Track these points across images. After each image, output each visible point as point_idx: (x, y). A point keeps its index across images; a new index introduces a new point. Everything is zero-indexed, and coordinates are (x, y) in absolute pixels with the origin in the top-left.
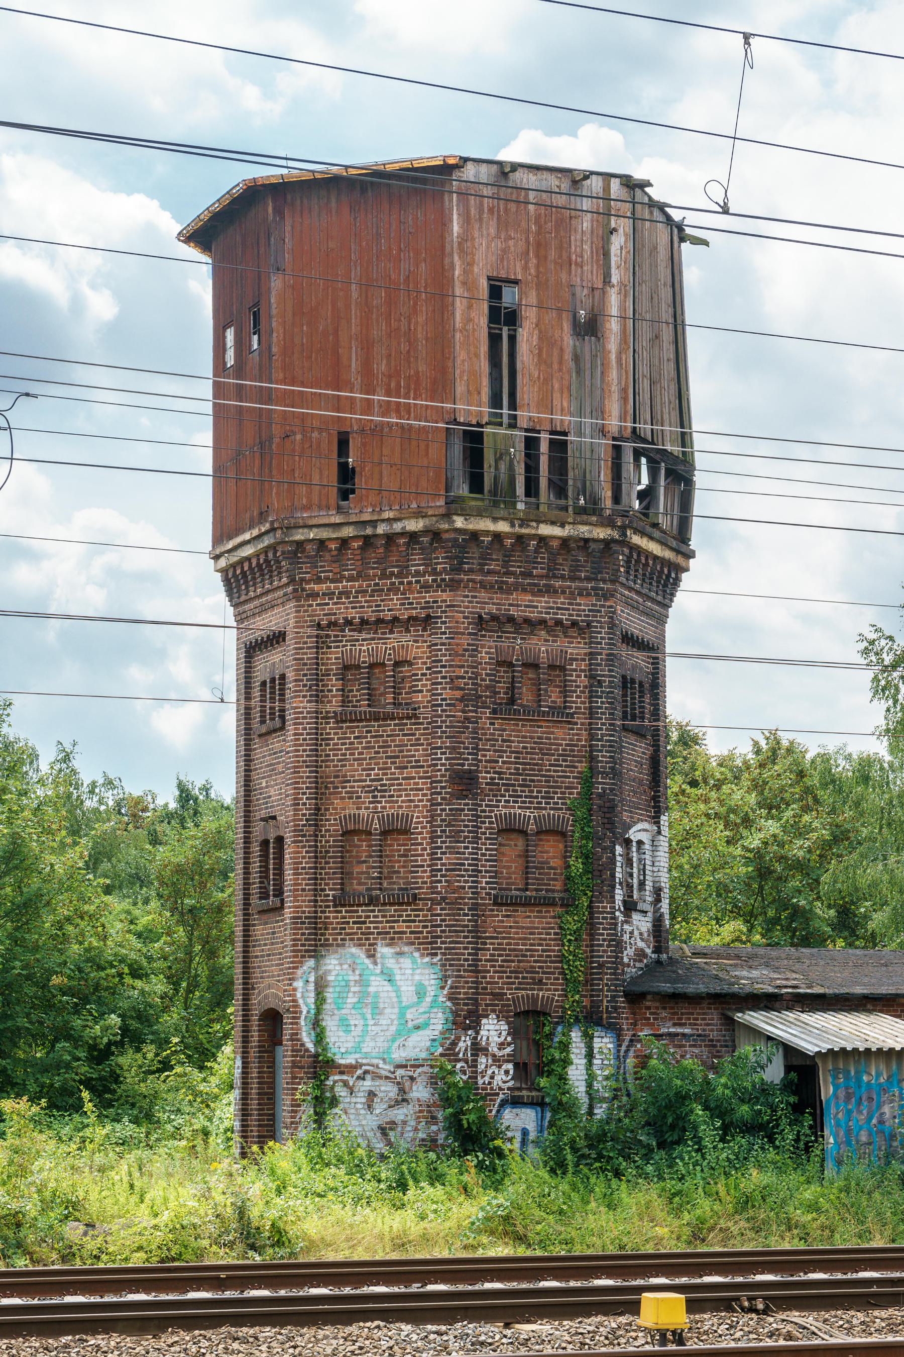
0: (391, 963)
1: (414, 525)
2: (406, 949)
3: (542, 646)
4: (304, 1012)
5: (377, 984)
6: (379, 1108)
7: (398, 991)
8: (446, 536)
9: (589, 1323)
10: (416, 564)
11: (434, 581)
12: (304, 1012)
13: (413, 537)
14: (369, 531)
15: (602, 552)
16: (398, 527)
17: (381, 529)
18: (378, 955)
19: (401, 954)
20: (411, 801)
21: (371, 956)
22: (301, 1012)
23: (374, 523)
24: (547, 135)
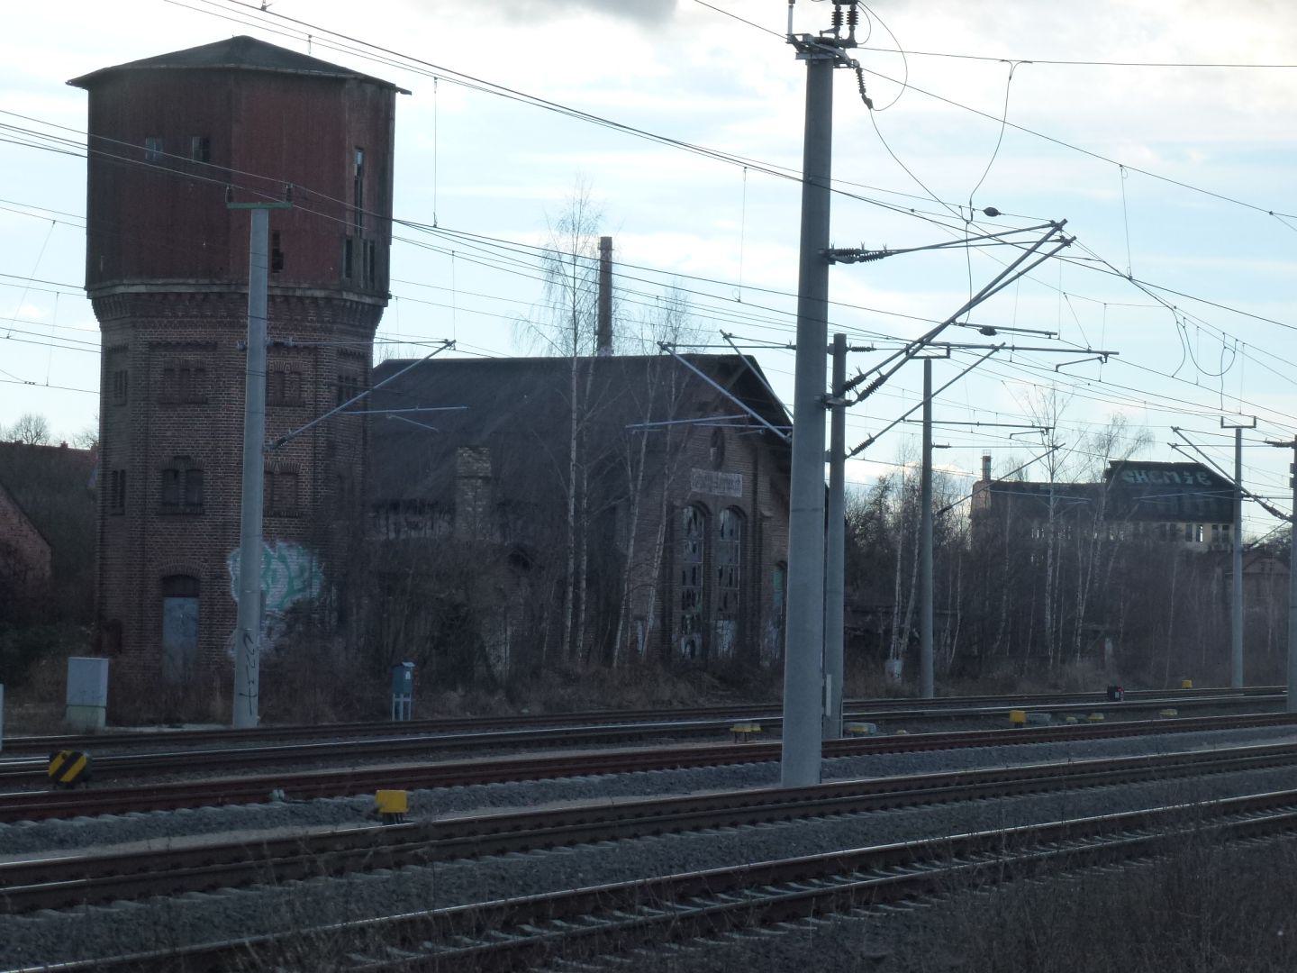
0: (285, 552)
1: (319, 294)
2: (294, 544)
3: (192, 357)
4: (234, 579)
5: (275, 564)
6: (275, 637)
7: (288, 568)
8: (335, 302)
9: (120, 787)
10: (312, 315)
11: (321, 327)
12: (234, 579)
13: (315, 300)
14: (290, 293)
15: (204, 300)
16: (309, 293)
17: (298, 293)
18: (277, 547)
19: (291, 546)
20: (300, 456)
21: (272, 546)
22: (231, 580)
23: (294, 289)
24: (242, 45)
